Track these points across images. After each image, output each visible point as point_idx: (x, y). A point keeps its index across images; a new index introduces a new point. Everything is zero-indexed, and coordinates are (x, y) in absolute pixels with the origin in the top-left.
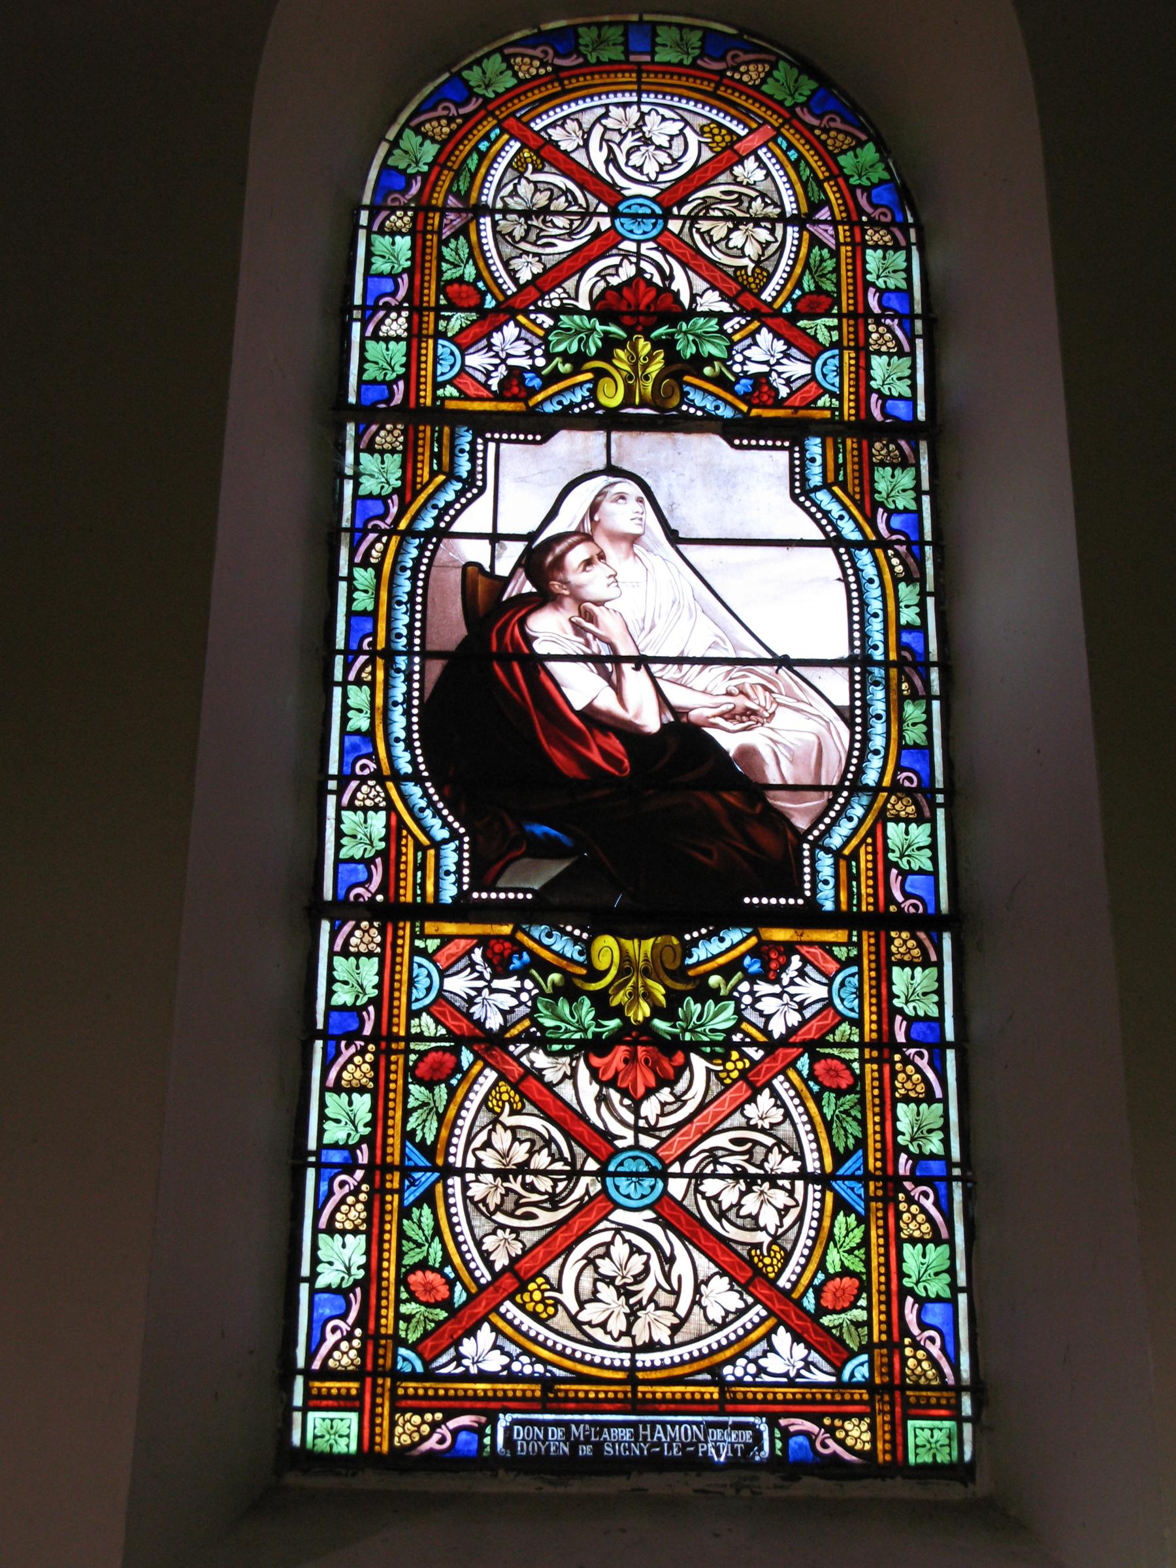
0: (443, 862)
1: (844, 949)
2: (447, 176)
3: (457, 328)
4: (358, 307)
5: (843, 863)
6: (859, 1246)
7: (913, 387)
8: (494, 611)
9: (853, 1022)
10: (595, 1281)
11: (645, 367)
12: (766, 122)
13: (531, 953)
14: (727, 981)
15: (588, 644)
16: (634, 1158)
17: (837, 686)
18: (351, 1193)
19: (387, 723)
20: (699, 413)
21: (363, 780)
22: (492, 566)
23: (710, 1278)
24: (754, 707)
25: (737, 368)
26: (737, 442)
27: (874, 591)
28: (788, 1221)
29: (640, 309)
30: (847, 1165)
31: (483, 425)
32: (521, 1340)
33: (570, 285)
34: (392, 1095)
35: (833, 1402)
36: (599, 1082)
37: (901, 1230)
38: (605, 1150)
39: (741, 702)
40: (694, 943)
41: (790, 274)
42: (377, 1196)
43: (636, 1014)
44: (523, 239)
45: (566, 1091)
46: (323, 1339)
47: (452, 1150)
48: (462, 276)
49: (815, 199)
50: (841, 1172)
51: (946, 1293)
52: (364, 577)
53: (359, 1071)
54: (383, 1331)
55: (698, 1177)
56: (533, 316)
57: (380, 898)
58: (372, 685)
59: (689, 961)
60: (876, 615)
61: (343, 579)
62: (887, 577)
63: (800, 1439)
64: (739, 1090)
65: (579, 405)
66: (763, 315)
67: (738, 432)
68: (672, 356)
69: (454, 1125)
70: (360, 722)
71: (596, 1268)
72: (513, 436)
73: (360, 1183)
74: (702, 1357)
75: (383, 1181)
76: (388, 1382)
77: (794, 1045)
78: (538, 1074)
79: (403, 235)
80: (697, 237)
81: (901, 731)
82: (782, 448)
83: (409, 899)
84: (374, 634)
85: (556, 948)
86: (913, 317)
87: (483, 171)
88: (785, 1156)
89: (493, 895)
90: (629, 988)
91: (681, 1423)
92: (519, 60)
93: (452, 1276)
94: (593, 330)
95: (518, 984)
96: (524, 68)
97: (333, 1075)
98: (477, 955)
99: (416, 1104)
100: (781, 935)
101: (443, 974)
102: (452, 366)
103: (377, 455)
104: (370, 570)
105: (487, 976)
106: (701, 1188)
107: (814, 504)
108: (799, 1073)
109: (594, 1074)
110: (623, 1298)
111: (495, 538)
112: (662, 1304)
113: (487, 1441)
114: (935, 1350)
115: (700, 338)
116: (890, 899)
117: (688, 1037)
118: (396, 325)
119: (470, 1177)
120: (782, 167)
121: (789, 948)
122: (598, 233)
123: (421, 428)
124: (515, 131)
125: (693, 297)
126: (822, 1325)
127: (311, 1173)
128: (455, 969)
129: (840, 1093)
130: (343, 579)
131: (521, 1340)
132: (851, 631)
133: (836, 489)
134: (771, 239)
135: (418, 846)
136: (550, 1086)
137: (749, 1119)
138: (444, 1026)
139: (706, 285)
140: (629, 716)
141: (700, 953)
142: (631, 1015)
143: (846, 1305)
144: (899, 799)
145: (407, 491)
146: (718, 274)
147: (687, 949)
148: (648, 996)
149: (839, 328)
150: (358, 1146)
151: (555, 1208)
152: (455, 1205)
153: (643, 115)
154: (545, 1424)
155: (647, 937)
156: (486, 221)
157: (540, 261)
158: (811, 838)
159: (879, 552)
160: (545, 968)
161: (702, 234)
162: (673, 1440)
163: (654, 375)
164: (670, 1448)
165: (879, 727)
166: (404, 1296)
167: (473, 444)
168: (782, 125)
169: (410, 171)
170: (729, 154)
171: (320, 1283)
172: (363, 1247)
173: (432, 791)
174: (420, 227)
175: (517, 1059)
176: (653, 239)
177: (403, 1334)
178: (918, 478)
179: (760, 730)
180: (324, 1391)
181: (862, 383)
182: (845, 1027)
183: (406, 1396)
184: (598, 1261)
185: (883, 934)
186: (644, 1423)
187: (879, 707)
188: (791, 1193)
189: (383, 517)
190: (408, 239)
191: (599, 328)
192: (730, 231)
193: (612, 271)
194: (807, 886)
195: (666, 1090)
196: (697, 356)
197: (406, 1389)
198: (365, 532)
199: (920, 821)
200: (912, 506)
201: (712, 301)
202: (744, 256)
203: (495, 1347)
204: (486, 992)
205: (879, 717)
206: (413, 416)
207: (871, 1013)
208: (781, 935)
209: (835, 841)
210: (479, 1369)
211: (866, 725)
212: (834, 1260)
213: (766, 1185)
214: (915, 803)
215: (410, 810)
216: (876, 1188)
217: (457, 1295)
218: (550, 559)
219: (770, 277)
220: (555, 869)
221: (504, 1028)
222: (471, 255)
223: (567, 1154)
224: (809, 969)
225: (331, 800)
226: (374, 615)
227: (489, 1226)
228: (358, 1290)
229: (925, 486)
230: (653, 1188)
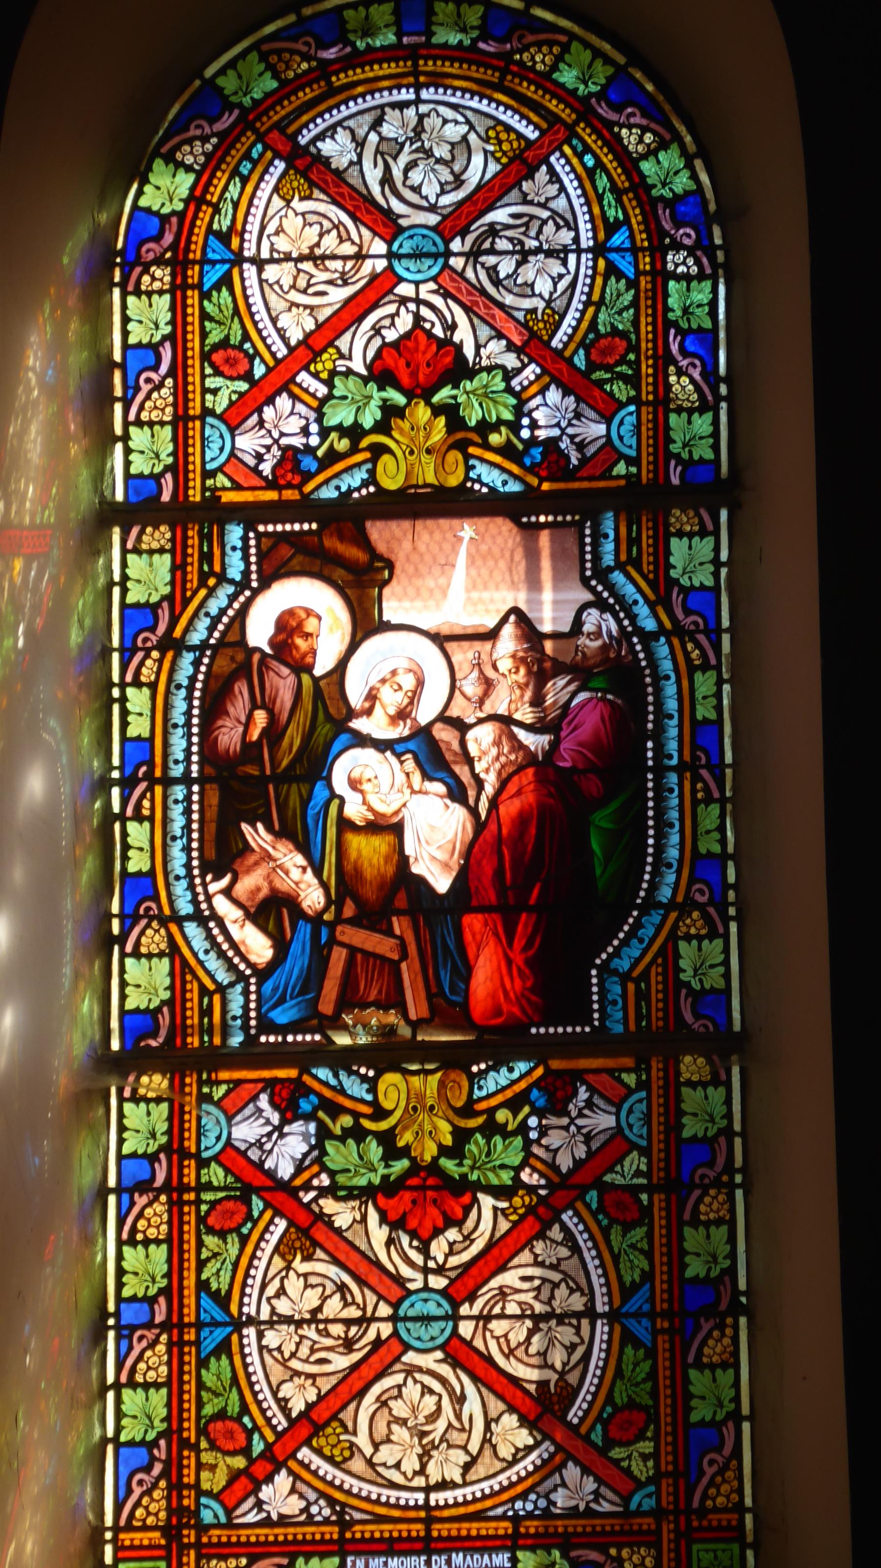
5: (631, 987)
10: (389, 1424)
13: (319, 1095)
20: (485, 490)
30: (219, 274)
36: (453, 344)
38: (396, 1292)
48: (227, 337)
50: (227, 266)
55: (360, 257)
58: (151, 819)
59: (477, 1094)
93: (250, 1426)
109: (384, 1219)
122: (472, 1298)
126: (611, 1460)
135: (204, 991)
145: (177, 599)
153: (421, 117)
160: (335, 1110)
167: (245, 539)
169: (166, 210)
183: (210, 1544)
191: (377, 396)
198: (134, 650)
201: (342, 1214)
204: (564, 424)
213: (553, 1323)
224: (596, 1100)
227: (552, 205)
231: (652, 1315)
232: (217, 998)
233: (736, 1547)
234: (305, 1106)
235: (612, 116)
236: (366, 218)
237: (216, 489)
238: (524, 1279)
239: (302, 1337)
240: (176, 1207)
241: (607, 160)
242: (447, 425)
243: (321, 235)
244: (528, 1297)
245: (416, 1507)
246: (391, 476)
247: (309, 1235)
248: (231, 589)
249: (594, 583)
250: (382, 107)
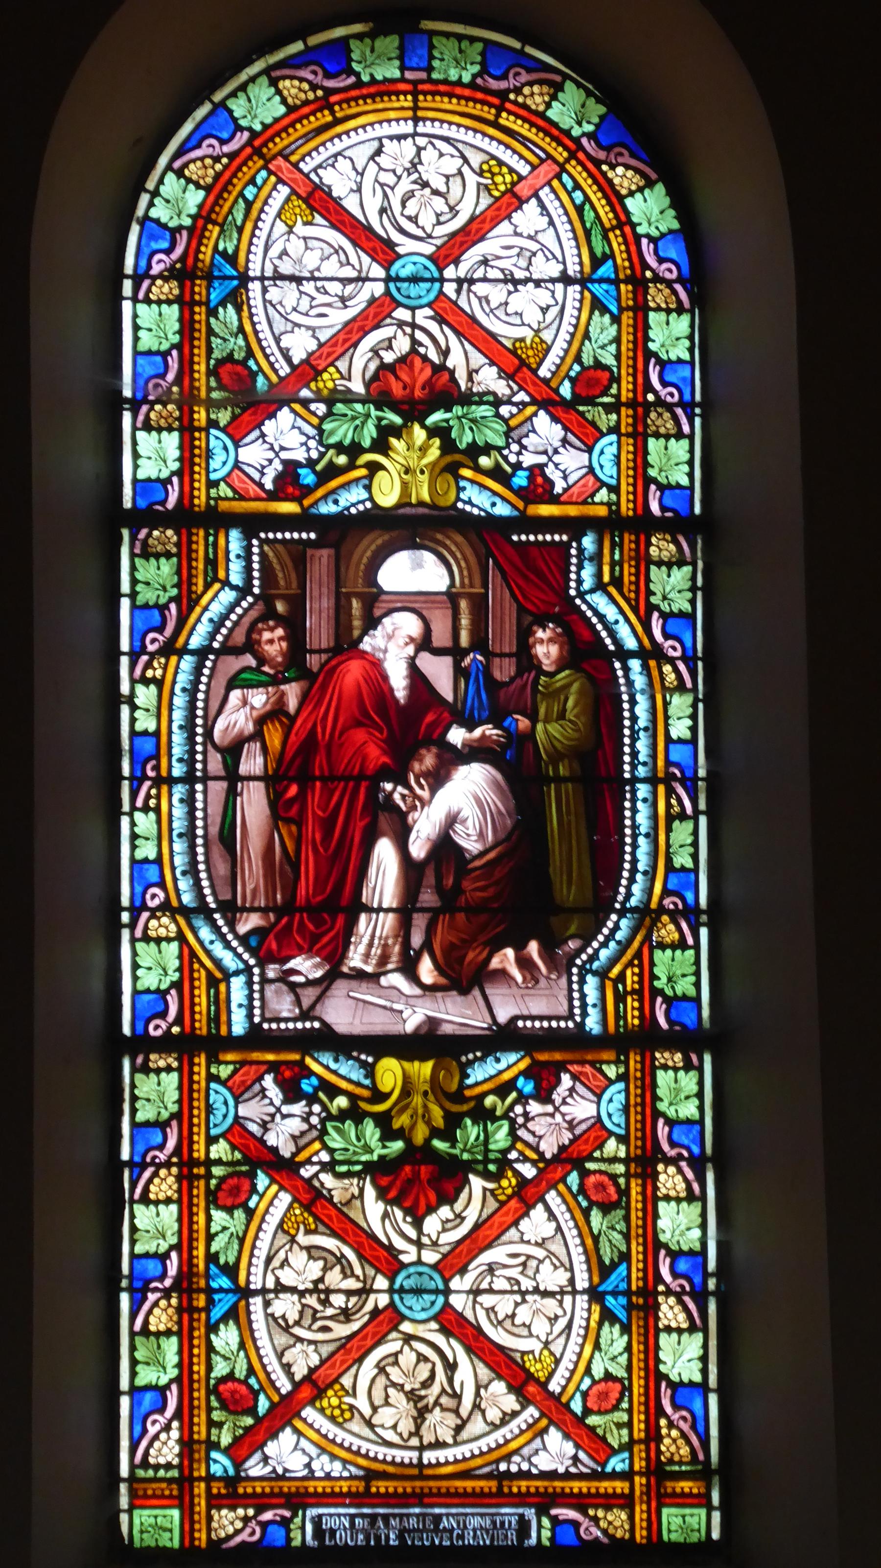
5: (609, 984)
10: (386, 1388)
12: (549, 156)
14: (503, 1101)
20: (355, 1054)
26: (317, 1025)
33: (342, 365)
36: (448, 369)
52: (145, 695)
55: (476, 1292)
57: (176, 1030)
59: (469, 1081)
71: (387, 1375)
99: (609, 348)
121: (273, 496)
126: (588, 1426)
151: (348, 1320)
160: (496, 473)
167: (584, 1014)
176: (430, 305)
191: (374, 413)
201: (490, 379)
204: (278, 1117)
206: (185, 518)
225: (126, 934)
231: (628, 1293)
232: (606, 578)
233: (703, 1512)
234: (306, 1086)
235: (602, 155)
236: (365, 244)
237: (220, 498)
239: (304, 1306)
240: (186, 1179)
241: (596, 197)
242: (441, 448)
243: (513, 1315)
244: (514, 1273)
245: (411, 1465)
246: (387, 493)
247: (517, 364)
248: (596, 965)
250: (456, 1443)
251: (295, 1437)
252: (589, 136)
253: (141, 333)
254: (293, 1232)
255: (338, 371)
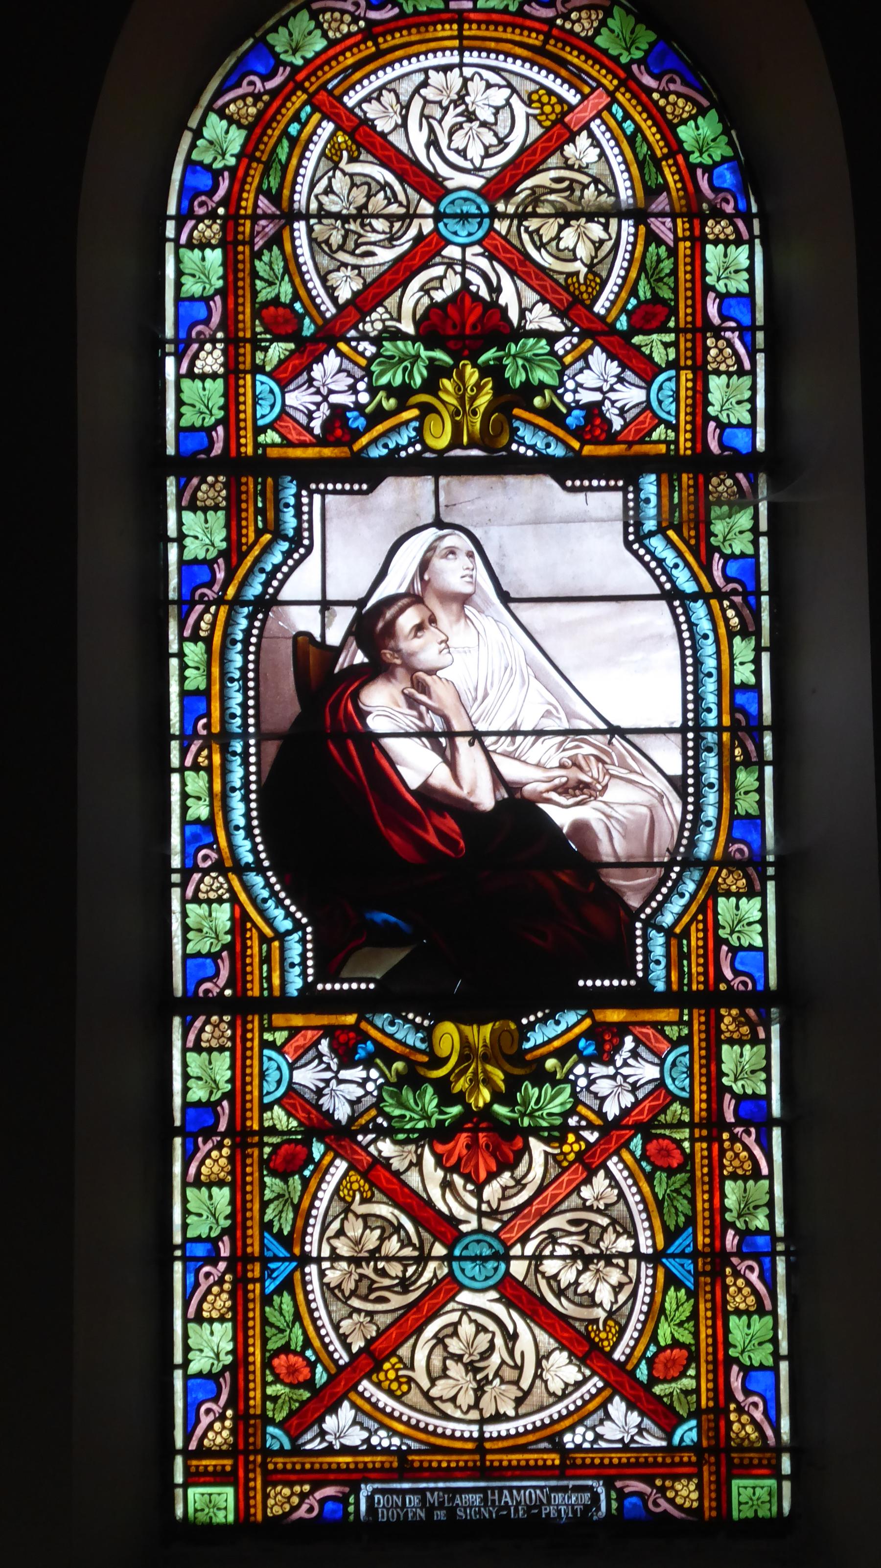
0: (288, 954)
1: (675, 1028)
2: (257, 170)
3: (275, 361)
4: (170, 342)
5: (674, 942)
6: (688, 1319)
7: (753, 412)
8: (325, 685)
9: (684, 1102)
10: (445, 1359)
11: (473, 399)
12: (600, 85)
13: (375, 1042)
14: (380, 404)
15: (421, 717)
16: (478, 1242)
17: (670, 756)
18: (215, 1283)
19: (226, 810)
20: (530, 453)
21: (206, 872)
22: (323, 635)
23: (550, 1353)
24: (587, 779)
25: (569, 398)
26: (569, 483)
27: (708, 648)
28: (622, 1298)
29: (466, 328)
30: (677, 1243)
31: (309, 474)
32: (379, 1416)
33: (391, 302)
34: (249, 1188)
35: (664, 1464)
37: (727, 1302)
39: (575, 774)
40: (531, 1027)
41: (625, 279)
42: (240, 1286)
43: (477, 1100)
44: (341, 248)
45: (413, 1179)
46: (198, 1421)
47: (308, 1239)
48: (278, 296)
49: (652, 183)
50: (670, 1251)
51: (769, 1362)
52: (194, 652)
53: (216, 1163)
54: (252, 1411)
55: (537, 1258)
56: (354, 344)
57: (228, 992)
58: (209, 770)
59: (527, 1046)
60: (710, 675)
61: (173, 655)
62: (722, 631)
63: (634, 1500)
64: (575, 1172)
65: (405, 448)
66: (599, 333)
67: (569, 471)
68: (501, 386)
69: (308, 1215)
70: (200, 810)
71: (445, 1347)
72: (339, 486)
73: (224, 1274)
74: (544, 1426)
75: (245, 1271)
76: (259, 1458)
77: (627, 1127)
78: (386, 1163)
79: (213, 247)
80: (525, 237)
81: (733, 800)
82: (616, 488)
83: (256, 993)
84: (208, 714)
85: (399, 1036)
86: (753, 328)
87: (294, 161)
88: (619, 1235)
89: (337, 986)
90: (469, 1074)
91: (525, 1488)
92: (328, 16)
93: (313, 1358)
94: (417, 356)
95: (364, 1074)
96: (334, 25)
97: (192, 1170)
98: (324, 1046)
100: (615, 1016)
101: (292, 1067)
102: (272, 406)
103: (199, 513)
104: (200, 644)
105: (334, 1067)
106: (541, 1268)
107: (648, 551)
108: (632, 1154)
109: (439, 1162)
110: (470, 1375)
111: (325, 605)
112: (507, 1378)
113: (351, 1509)
114: (758, 1415)
115: (530, 362)
116: (720, 976)
117: (526, 1122)
118: (211, 360)
119: (326, 1265)
120: (618, 145)
121: (623, 1029)
122: (420, 238)
123: (244, 480)
124: (327, 109)
125: (522, 312)
127: (178, 1267)
128: (303, 1061)
129: (671, 1172)
130: (173, 655)
131: (379, 1416)
132: (685, 693)
133: (671, 533)
134: (604, 236)
135: (263, 939)
136: (397, 1174)
137: (585, 1200)
138: (296, 1118)
139: (536, 297)
140: (463, 793)
141: (536, 1037)
142: (472, 1101)
143: (676, 1374)
144: (730, 872)
145: (234, 553)
146: (548, 283)
147: (523, 1032)
148: (488, 1081)
149: (675, 344)
150: (219, 1238)
151: (406, 1291)
152: (312, 1291)
153: (466, 81)
154: (404, 1492)
155: (486, 1023)
156: (300, 226)
157: (359, 274)
158: (643, 916)
159: (714, 603)
160: (389, 1057)
161: (530, 234)
162: (519, 1503)
163: (482, 409)
164: (516, 1511)
165: (711, 797)
166: (270, 1378)
167: (298, 496)
168: (617, 89)
169: (217, 165)
170: (559, 131)
171: (193, 1368)
172: (230, 1334)
173: (273, 880)
174: (230, 238)
175: (365, 1149)
176: (479, 242)
177: (270, 1414)
178: (756, 517)
179: (594, 804)
180: (201, 1469)
181: (699, 410)
182: (676, 1107)
183: (275, 1470)
184: (447, 1341)
185: (713, 1011)
186: (493, 1489)
187: (712, 775)
188: (625, 1271)
189: (210, 585)
190: (218, 252)
191: (424, 354)
192: (561, 228)
193: (436, 284)
194: (640, 966)
195: (507, 1175)
196: (527, 383)
197: (276, 1464)
198: (192, 604)
199: (750, 894)
200: (750, 550)
201: (543, 317)
202: (575, 259)
203: (355, 1423)
204: (333, 1083)
205: (711, 786)
207: (701, 1092)
208: (615, 1016)
209: (667, 919)
210: (342, 1445)
211: (698, 795)
212: (665, 1333)
213: (602, 1264)
214: (747, 876)
215: (253, 899)
216: (704, 1264)
217: (318, 1376)
218: (380, 625)
219: (604, 283)
220: (395, 957)
221: (352, 1119)
222: (286, 270)
223: (415, 1240)
224: (642, 1050)
225: (176, 893)
226: (206, 694)
227: (345, 1311)
228: (227, 1374)
229: (763, 526)
230: (496, 1269)
238: (572, 1222)
248: (285, 546)
249: (636, 546)
251: (353, 1412)
252: (639, 62)
253: (184, 279)
254: (591, 277)
255: (387, 311)
